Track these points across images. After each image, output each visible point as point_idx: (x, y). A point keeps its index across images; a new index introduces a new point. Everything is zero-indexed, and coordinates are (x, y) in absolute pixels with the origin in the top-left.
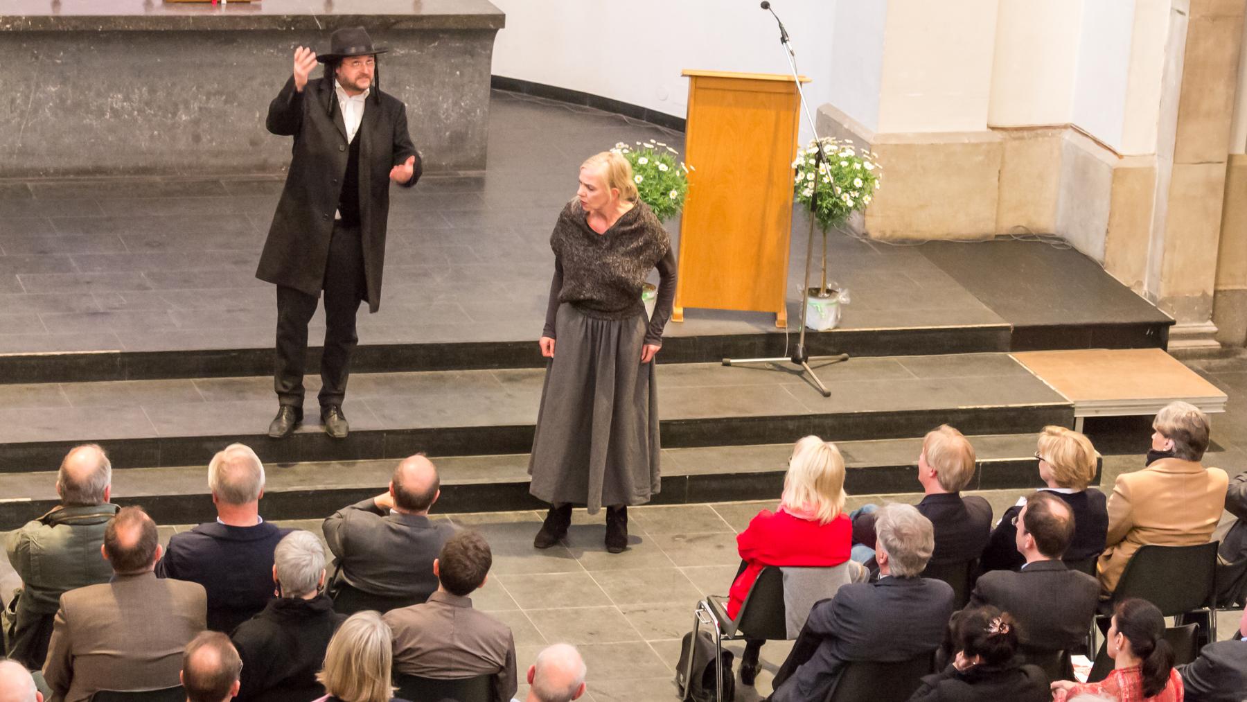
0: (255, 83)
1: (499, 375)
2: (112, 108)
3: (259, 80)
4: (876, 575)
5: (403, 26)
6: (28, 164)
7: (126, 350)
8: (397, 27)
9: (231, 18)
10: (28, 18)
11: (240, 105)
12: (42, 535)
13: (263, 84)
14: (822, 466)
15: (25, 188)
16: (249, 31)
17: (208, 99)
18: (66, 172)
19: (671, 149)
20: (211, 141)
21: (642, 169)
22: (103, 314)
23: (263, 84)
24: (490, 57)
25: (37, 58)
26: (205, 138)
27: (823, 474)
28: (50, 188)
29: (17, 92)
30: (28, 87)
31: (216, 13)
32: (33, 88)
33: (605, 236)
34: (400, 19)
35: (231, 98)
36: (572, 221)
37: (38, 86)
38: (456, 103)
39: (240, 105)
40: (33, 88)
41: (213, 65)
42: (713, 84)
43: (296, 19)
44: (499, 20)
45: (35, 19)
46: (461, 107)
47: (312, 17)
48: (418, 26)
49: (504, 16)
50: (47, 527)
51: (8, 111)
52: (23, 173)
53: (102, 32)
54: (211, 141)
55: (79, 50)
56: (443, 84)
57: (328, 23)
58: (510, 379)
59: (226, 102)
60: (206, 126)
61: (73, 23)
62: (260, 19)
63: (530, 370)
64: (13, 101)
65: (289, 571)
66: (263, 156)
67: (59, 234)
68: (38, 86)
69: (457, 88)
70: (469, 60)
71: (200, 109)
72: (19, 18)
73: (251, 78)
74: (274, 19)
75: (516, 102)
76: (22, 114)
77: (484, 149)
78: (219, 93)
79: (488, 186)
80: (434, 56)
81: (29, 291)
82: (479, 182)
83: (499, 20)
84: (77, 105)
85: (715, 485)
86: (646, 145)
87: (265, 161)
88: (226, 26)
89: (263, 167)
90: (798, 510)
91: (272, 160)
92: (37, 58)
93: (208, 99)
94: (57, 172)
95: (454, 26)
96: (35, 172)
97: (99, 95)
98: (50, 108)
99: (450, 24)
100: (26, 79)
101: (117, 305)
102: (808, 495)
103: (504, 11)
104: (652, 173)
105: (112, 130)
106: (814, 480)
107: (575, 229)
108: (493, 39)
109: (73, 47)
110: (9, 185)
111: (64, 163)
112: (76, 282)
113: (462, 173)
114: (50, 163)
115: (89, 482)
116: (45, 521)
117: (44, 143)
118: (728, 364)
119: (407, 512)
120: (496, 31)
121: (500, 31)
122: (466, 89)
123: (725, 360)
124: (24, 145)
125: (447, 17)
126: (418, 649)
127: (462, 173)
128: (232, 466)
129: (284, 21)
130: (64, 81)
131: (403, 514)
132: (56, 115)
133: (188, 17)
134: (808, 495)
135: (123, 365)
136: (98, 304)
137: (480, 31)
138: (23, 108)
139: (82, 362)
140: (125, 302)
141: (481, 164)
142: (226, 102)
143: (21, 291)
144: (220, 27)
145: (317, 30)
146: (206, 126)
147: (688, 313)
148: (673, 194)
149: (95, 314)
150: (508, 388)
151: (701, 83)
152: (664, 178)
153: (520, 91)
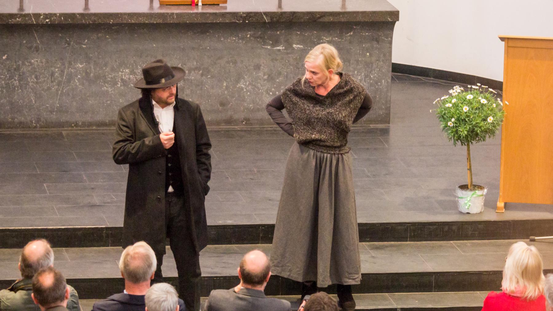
0: (223, 62)
1: (369, 246)
2: (122, 79)
3: (225, 59)
5: (326, 19)
6: (64, 118)
7: (110, 226)
8: (321, 20)
9: (203, 14)
10: (62, 15)
11: (212, 77)
12: (9, 297)
13: (228, 62)
14: (526, 261)
15: (61, 134)
16: (217, 24)
17: (190, 73)
18: (90, 124)
19: (491, 90)
21: (470, 103)
22: (99, 206)
23: (228, 62)
24: (391, 43)
25: (69, 44)
27: (526, 268)
28: (78, 134)
29: (56, 68)
30: (63, 64)
31: (195, 11)
32: (67, 65)
34: (324, 14)
35: (206, 72)
37: (70, 63)
38: (366, 76)
39: (212, 77)
40: (67, 65)
41: (193, 48)
42: (519, 44)
43: (249, 15)
44: (395, 15)
45: (66, 16)
46: (370, 79)
47: (261, 13)
48: (336, 19)
49: (398, 12)
50: (13, 293)
51: (49, 81)
52: (61, 125)
53: (113, 25)
55: (98, 38)
56: (357, 61)
57: (272, 18)
58: (377, 248)
61: (93, 18)
62: (223, 15)
63: (393, 243)
64: (52, 74)
65: (154, 306)
66: (230, 113)
67: (78, 161)
68: (70, 63)
69: (368, 65)
70: (375, 44)
72: (55, 14)
73: (219, 58)
74: (234, 15)
75: (424, 83)
76: (59, 84)
77: (388, 109)
79: (392, 133)
80: (350, 42)
81: (50, 193)
82: (385, 132)
83: (395, 15)
84: (97, 77)
86: (473, 87)
87: (231, 117)
88: (200, 20)
89: (229, 122)
90: (513, 292)
91: (236, 117)
92: (69, 44)
94: (84, 124)
95: (362, 20)
96: (68, 124)
97: (113, 69)
98: (79, 80)
99: (360, 18)
100: (62, 59)
101: (109, 201)
102: (518, 282)
103: (399, 10)
104: (476, 105)
105: (122, 95)
106: (521, 272)
108: (392, 29)
109: (94, 36)
110: (49, 132)
111: (88, 118)
112: (85, 188)
113: (372, 126)
114: (78, 118)
115: (38, 261)
116: (11, 290)
117: (75, 104)
118: (533, 240)
119: (249, 287)
120: (395, 22)
121: (397, 22)
122: (374, 66)
123: (532, 237)
124: (61, 107)
125: (357, 13)
127: (372, 126)
128: (133, 258)
129: (241, 17)
130: (88, 59)
131: (247, 289)
132: (83, 84)
133: (173, 14)
134: (518, 282)
135: (107, 236)
136: (96, 200)
137: (382, 24)
138: (60, 79)
139: (79, 233)
140: (115, 199)
141: (386, 119)
142: (202, 75)
143: (46, 193)
144: (196, 21)
145: (265, 23)
147: (507, 206)
148: (490, 119)
149: (93, 206)
150: (373, 253)
151: (511, 44)
152: (485, 109)
153: (427, 76)
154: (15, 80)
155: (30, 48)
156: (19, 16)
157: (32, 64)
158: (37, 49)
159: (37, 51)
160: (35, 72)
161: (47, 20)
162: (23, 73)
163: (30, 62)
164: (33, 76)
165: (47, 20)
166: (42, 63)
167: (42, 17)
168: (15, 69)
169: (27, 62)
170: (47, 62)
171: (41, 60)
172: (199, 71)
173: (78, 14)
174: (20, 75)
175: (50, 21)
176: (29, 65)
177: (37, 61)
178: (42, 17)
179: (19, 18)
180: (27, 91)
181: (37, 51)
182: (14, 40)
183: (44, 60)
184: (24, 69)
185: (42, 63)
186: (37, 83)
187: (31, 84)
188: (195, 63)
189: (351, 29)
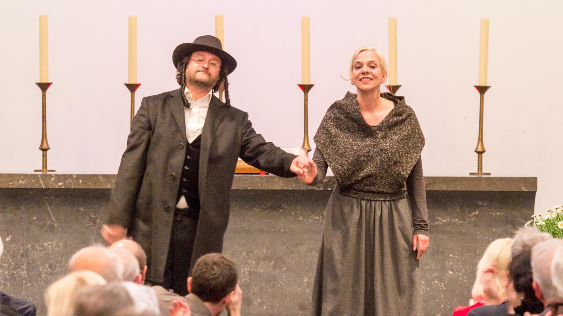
4: (323, 179)
11: (288, 270)
17: (258, 264)
20: (262, 304)
25: (94, 222)
26: (256, 302)
33: (379, 128)
36: (347, 117)
39: (288, 270)
41: (262, 231)
49: (536, 179)
54: (262, 304)
59: (275, 267)
60: (256, 290)
71: (250, 273)
73: (297, 245)
78: (267, 258)
85: (369, 286)
92: (94, 222)
93: (258, 264)
107: (350, 124)
126: (26, 303)
142: (275, 267)
146: (256, 290)
154: (22, 270)
155: (42, 227)
156: (22, 177)
157: (44, 248)
158: (51, 228)
159: (52, 231)
160: (49, 259)
161: (60, 184)
162: (34, 261)
163: (43, 246)
164: (47, 265)
165: (60, 184)
166: (58, 247)
167: (53, 179)
168: (22, 255)
169: (40, 246)
170: (66, 246)
171: (57, 244)
172: (270, 262)
173: (101, 175)
174: (29, 263)
175: (64, 184)
176: (40, 250)
177: (52, 245)
178: (53, 179)
179: (23, 180)
180: (39, 285)
181: (52, 231)
182: (21, 216)
183: (61, 244)
184: (34, 255)
185: (58, 247)
186: (51, 274)
187: (43, 276)
188: (265, 251)
189: (476, 206)
